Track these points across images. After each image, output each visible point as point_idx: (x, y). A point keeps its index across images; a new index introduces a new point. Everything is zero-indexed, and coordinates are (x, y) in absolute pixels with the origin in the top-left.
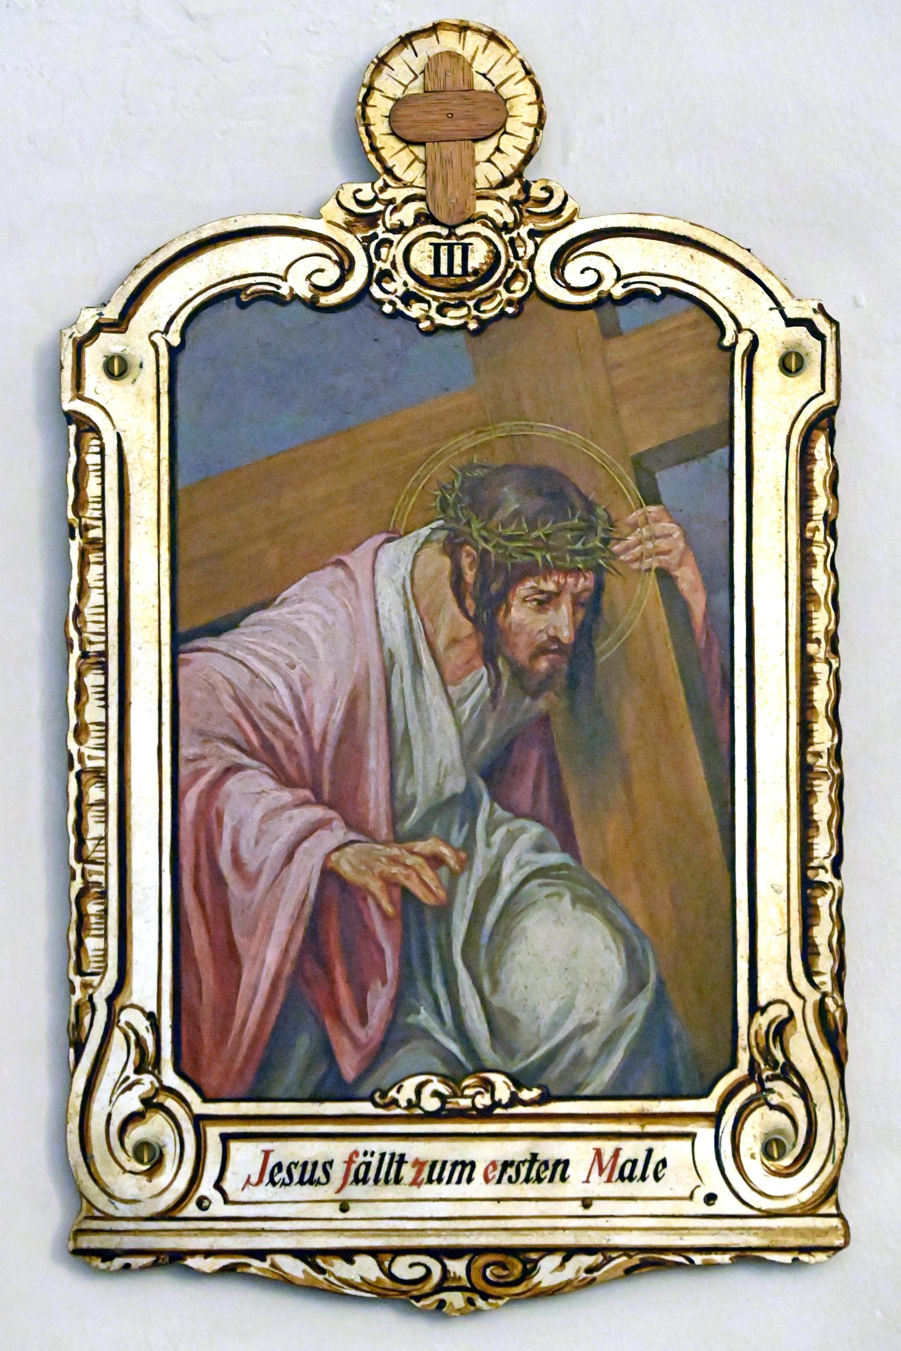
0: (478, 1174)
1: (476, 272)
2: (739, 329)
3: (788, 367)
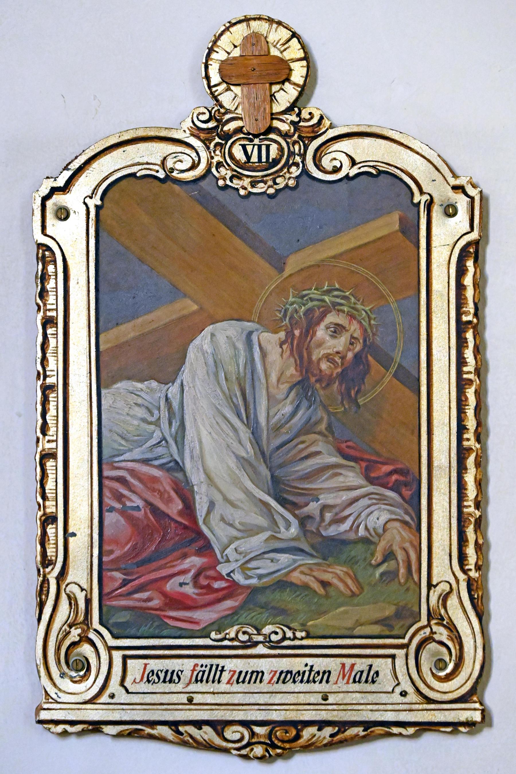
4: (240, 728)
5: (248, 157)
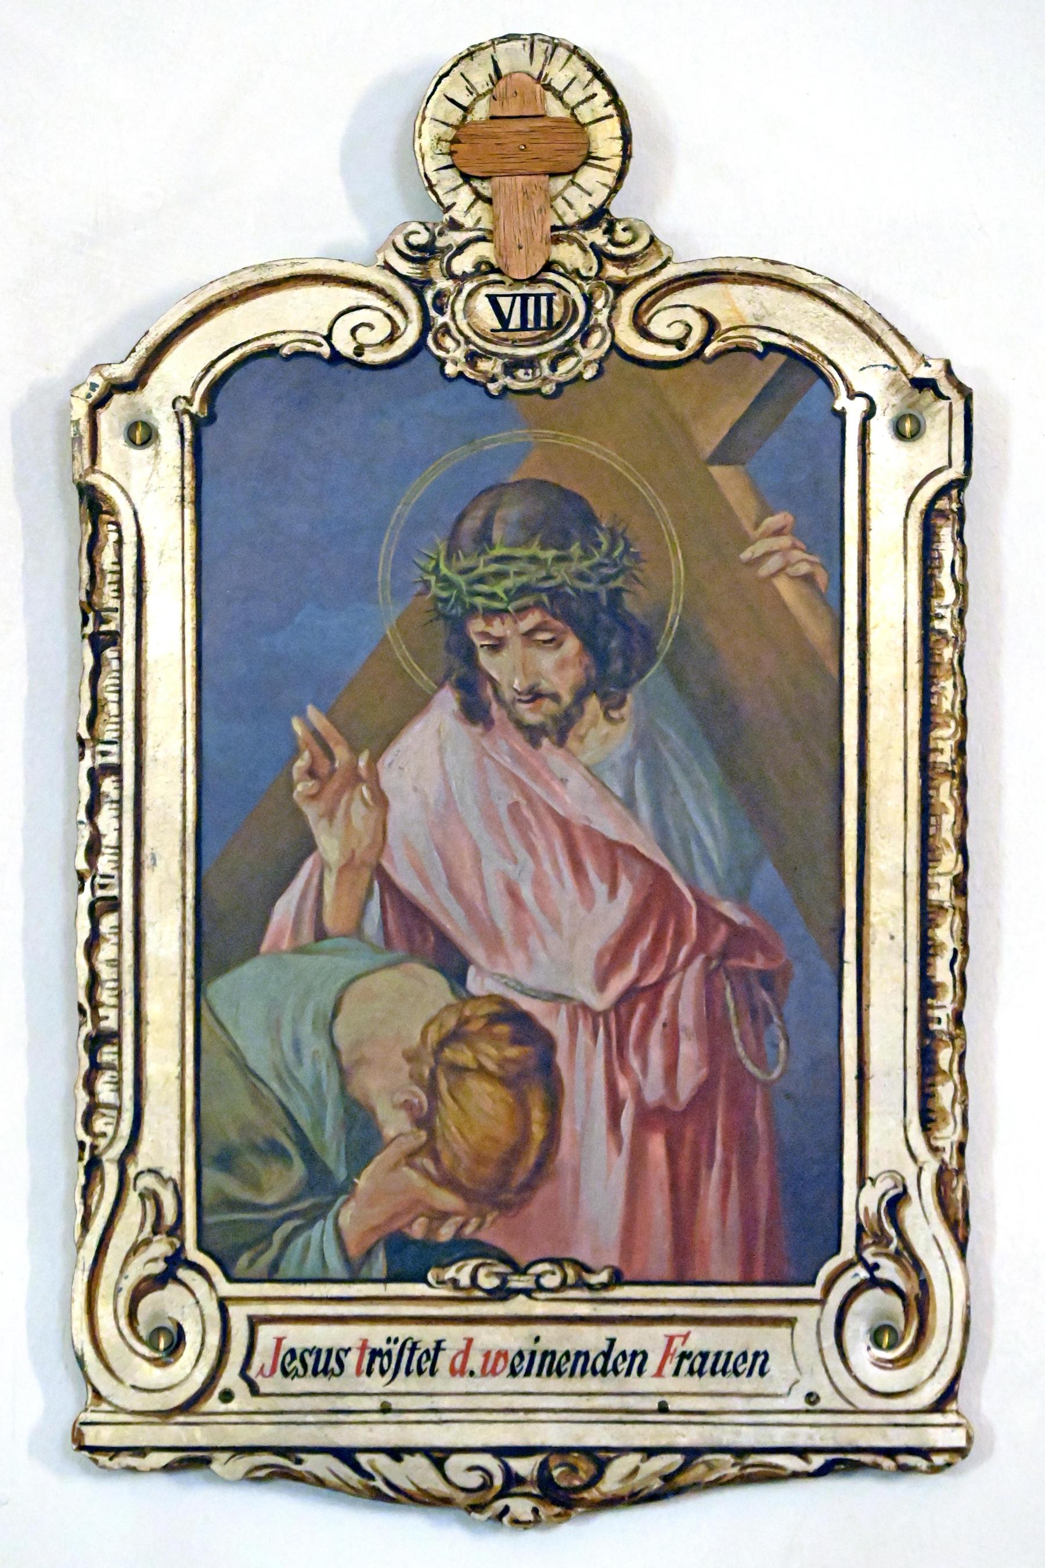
0: (351, 1360)
5: (504, 321)
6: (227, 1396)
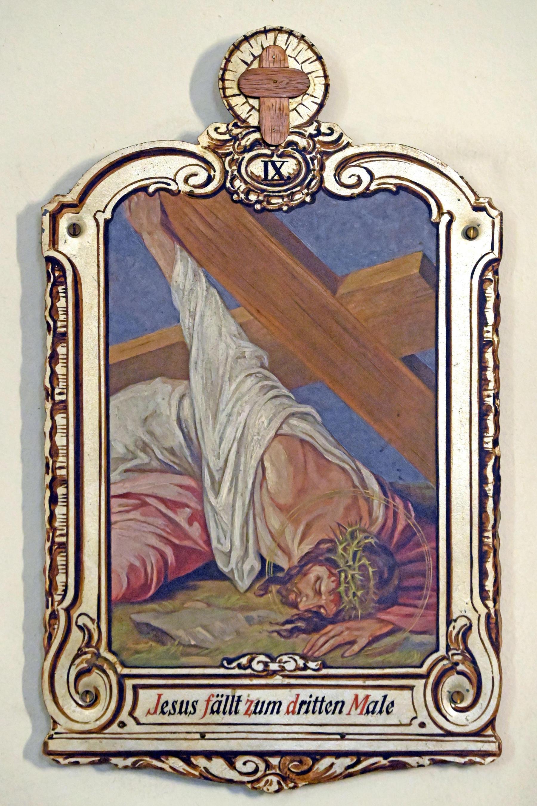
0: (283, 709)
1: (289, 178)
2: (441, 213)
3: (469, 236)
4: (255, 759)
6: (122, 725)
